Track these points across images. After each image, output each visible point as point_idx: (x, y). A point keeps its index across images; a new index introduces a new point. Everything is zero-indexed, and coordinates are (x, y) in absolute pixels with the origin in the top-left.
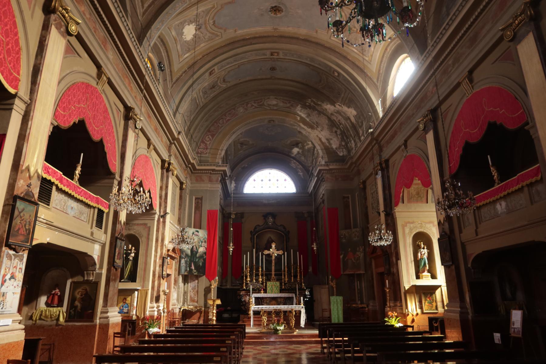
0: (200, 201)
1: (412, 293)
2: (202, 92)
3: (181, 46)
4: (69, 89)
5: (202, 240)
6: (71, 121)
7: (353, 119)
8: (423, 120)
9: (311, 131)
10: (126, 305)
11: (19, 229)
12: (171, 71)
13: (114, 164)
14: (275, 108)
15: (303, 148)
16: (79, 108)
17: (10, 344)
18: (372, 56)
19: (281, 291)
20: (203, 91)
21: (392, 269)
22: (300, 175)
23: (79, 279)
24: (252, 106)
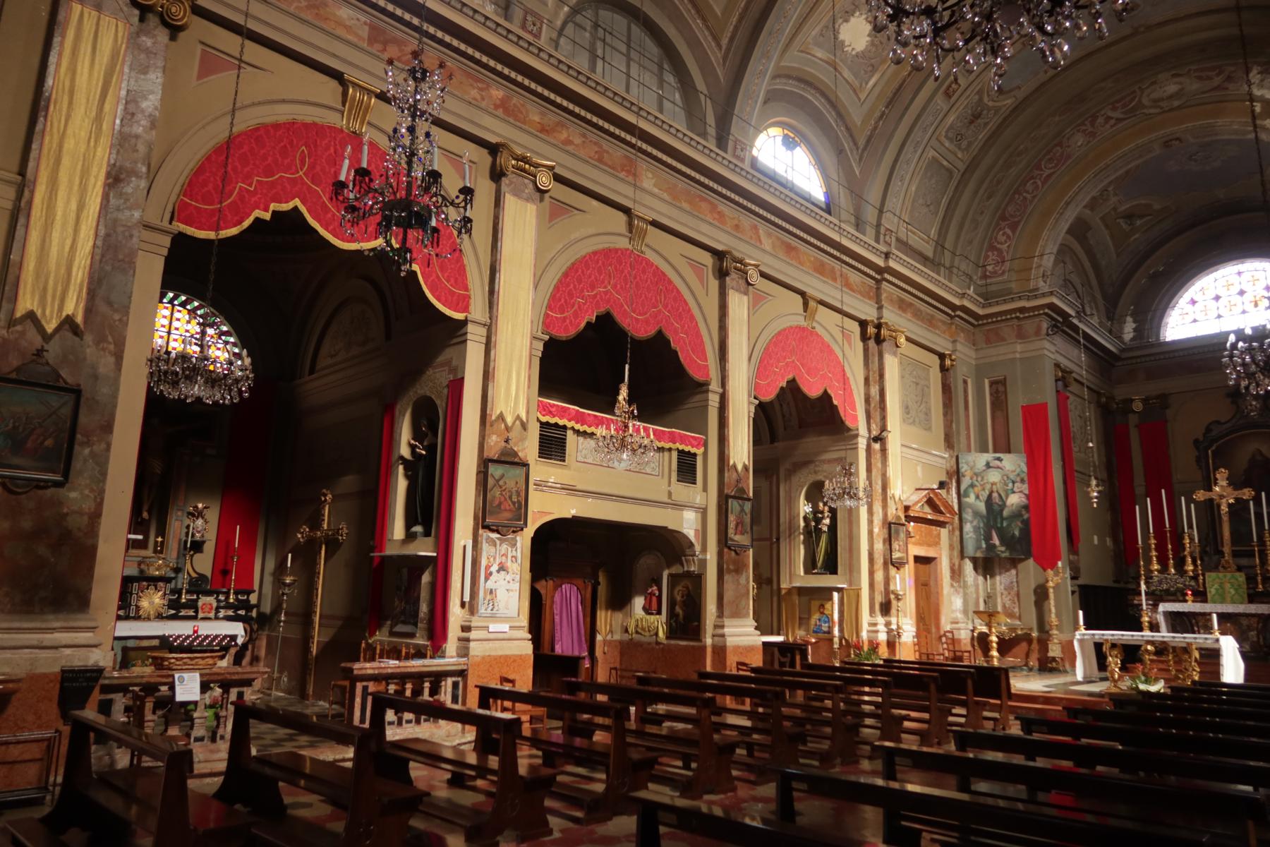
0: (1001, 388)
2: (951, 140)
3: (850, 69)
4: (566, 275)
5: (1012, 476)
6: (579, 324)
10: (824, 618)
11: (500, 504)
12: (848, 129)
13: (703, 365)
14: (1176, 103)
16: (595, 296)
17: (506, 657)
19: (1252, 599)
20: (950, 135)
23: (676, 569)
24: (1109, 118)
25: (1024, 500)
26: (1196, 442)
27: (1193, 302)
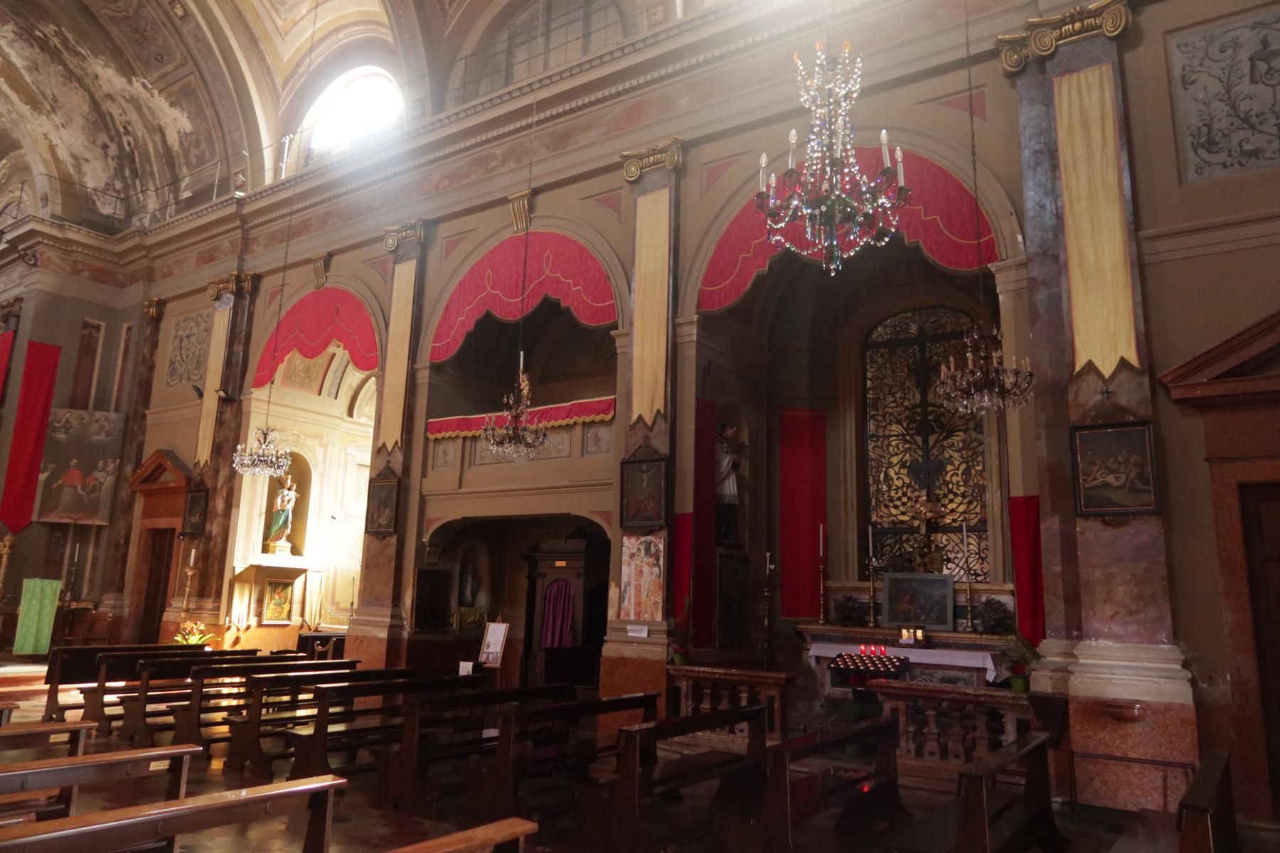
1: (248, 581)
7: (173, 139)
8: (397, 231)
9: (29, 115)
18: (295, 23)
21: (208, 526)
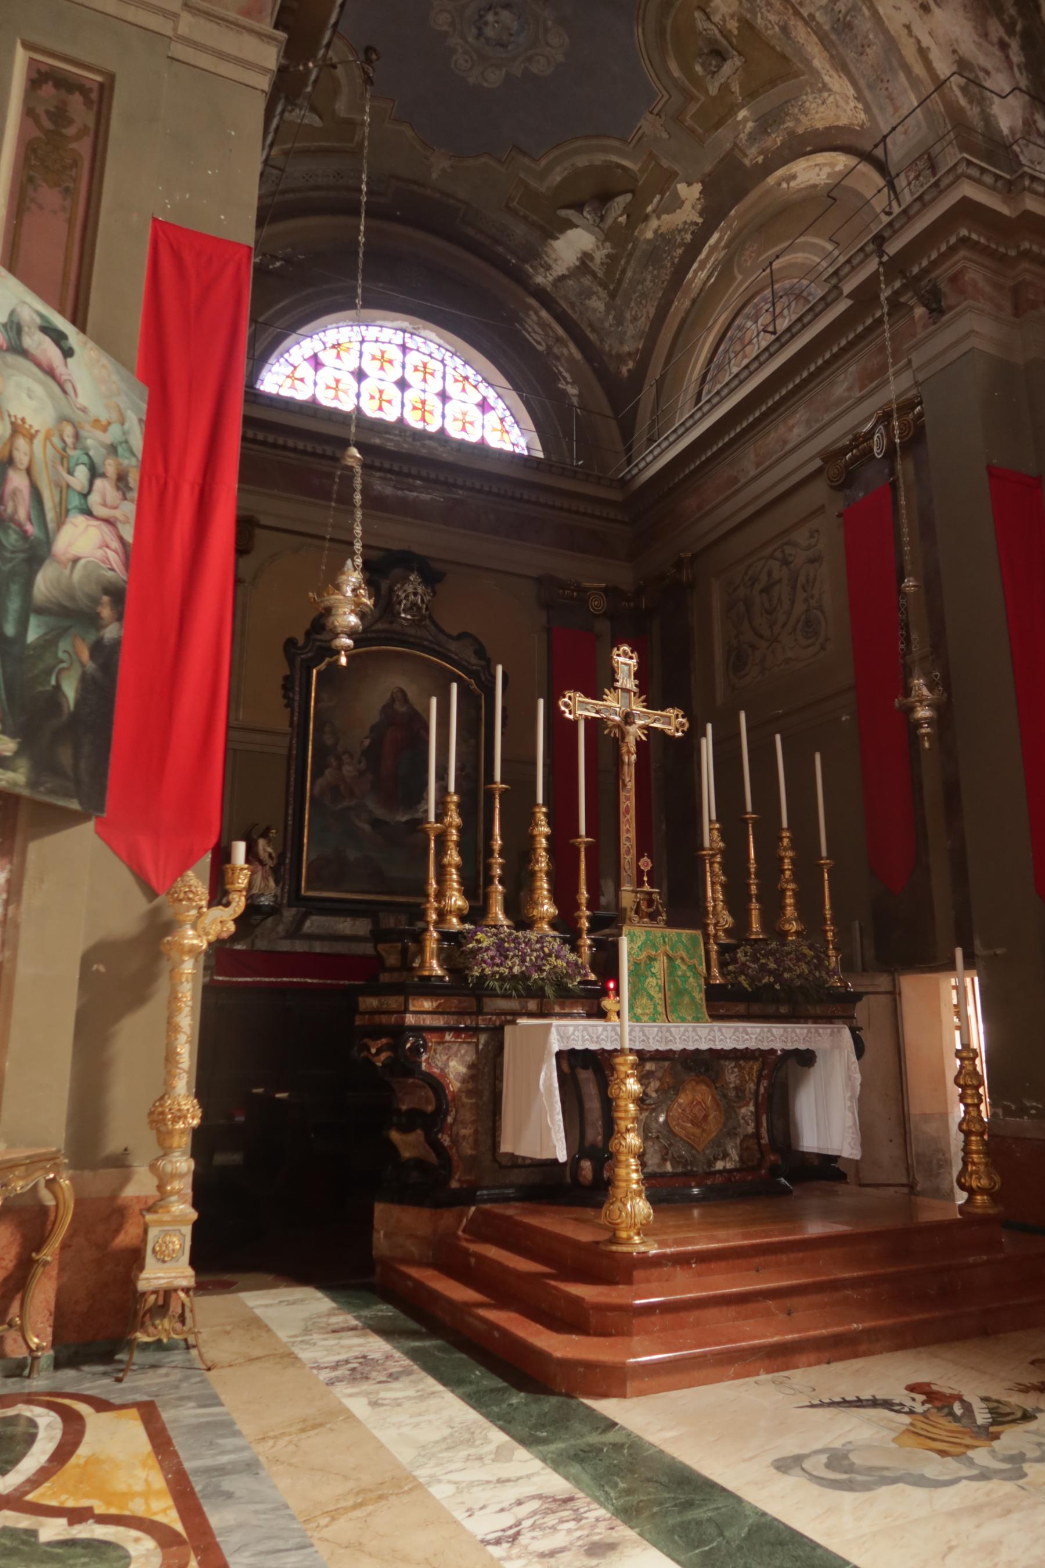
0: (81, 114)
15: (618, 238)
19: (722, 1002)
22: (564, 393)
25: (115, 568)
26: (290, 643)
27: (316, 363)
